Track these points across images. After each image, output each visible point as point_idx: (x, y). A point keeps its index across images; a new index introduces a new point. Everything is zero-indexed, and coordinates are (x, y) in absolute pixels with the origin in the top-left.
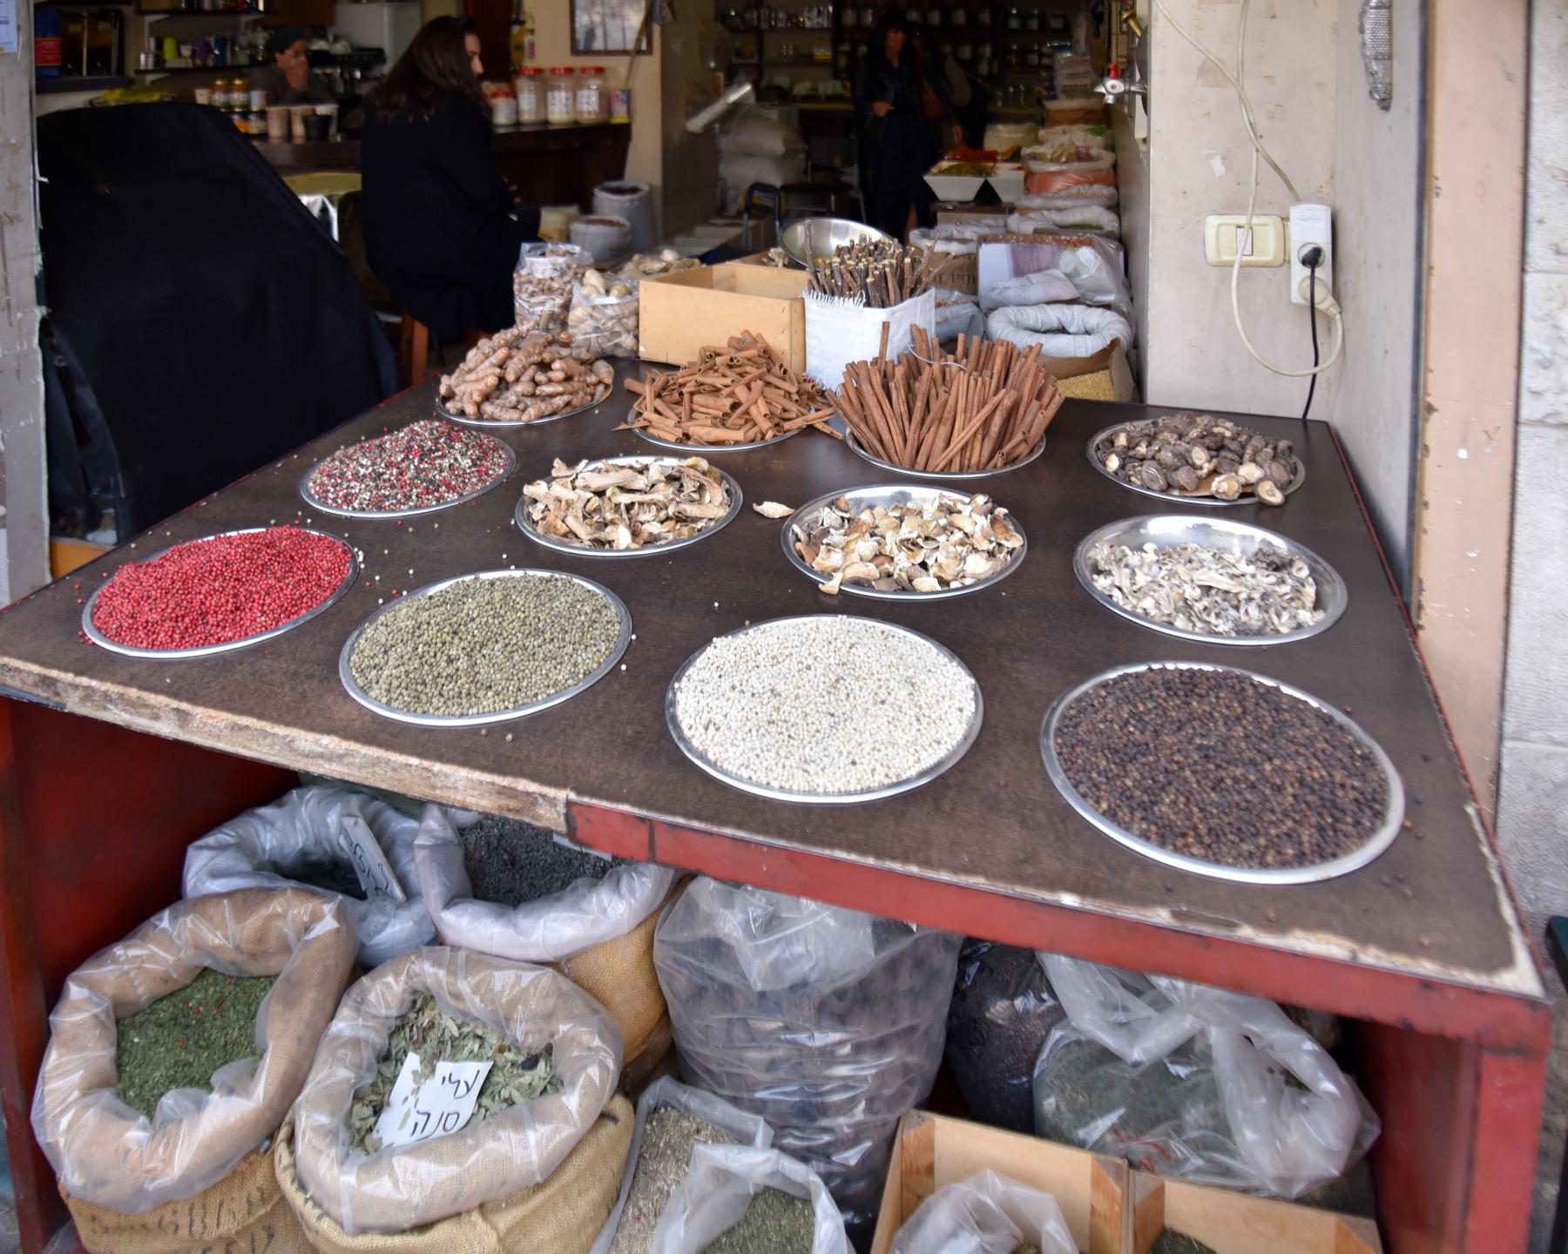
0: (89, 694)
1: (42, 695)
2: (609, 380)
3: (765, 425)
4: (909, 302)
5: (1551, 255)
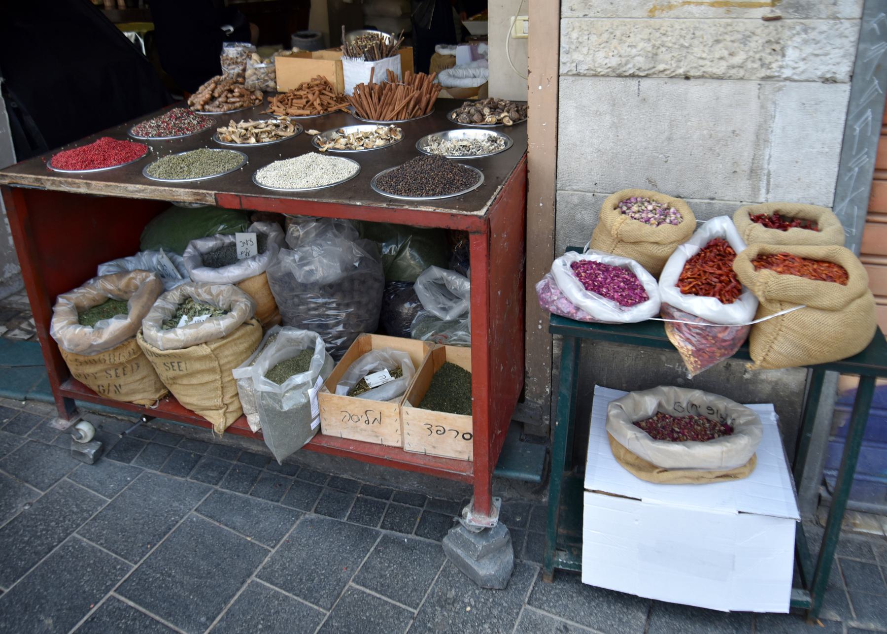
0: (54, 183)
1: (36, 185)
2: (261, 98)
3: (319, 108)
4: (385, 60)
5: (569, 10)
